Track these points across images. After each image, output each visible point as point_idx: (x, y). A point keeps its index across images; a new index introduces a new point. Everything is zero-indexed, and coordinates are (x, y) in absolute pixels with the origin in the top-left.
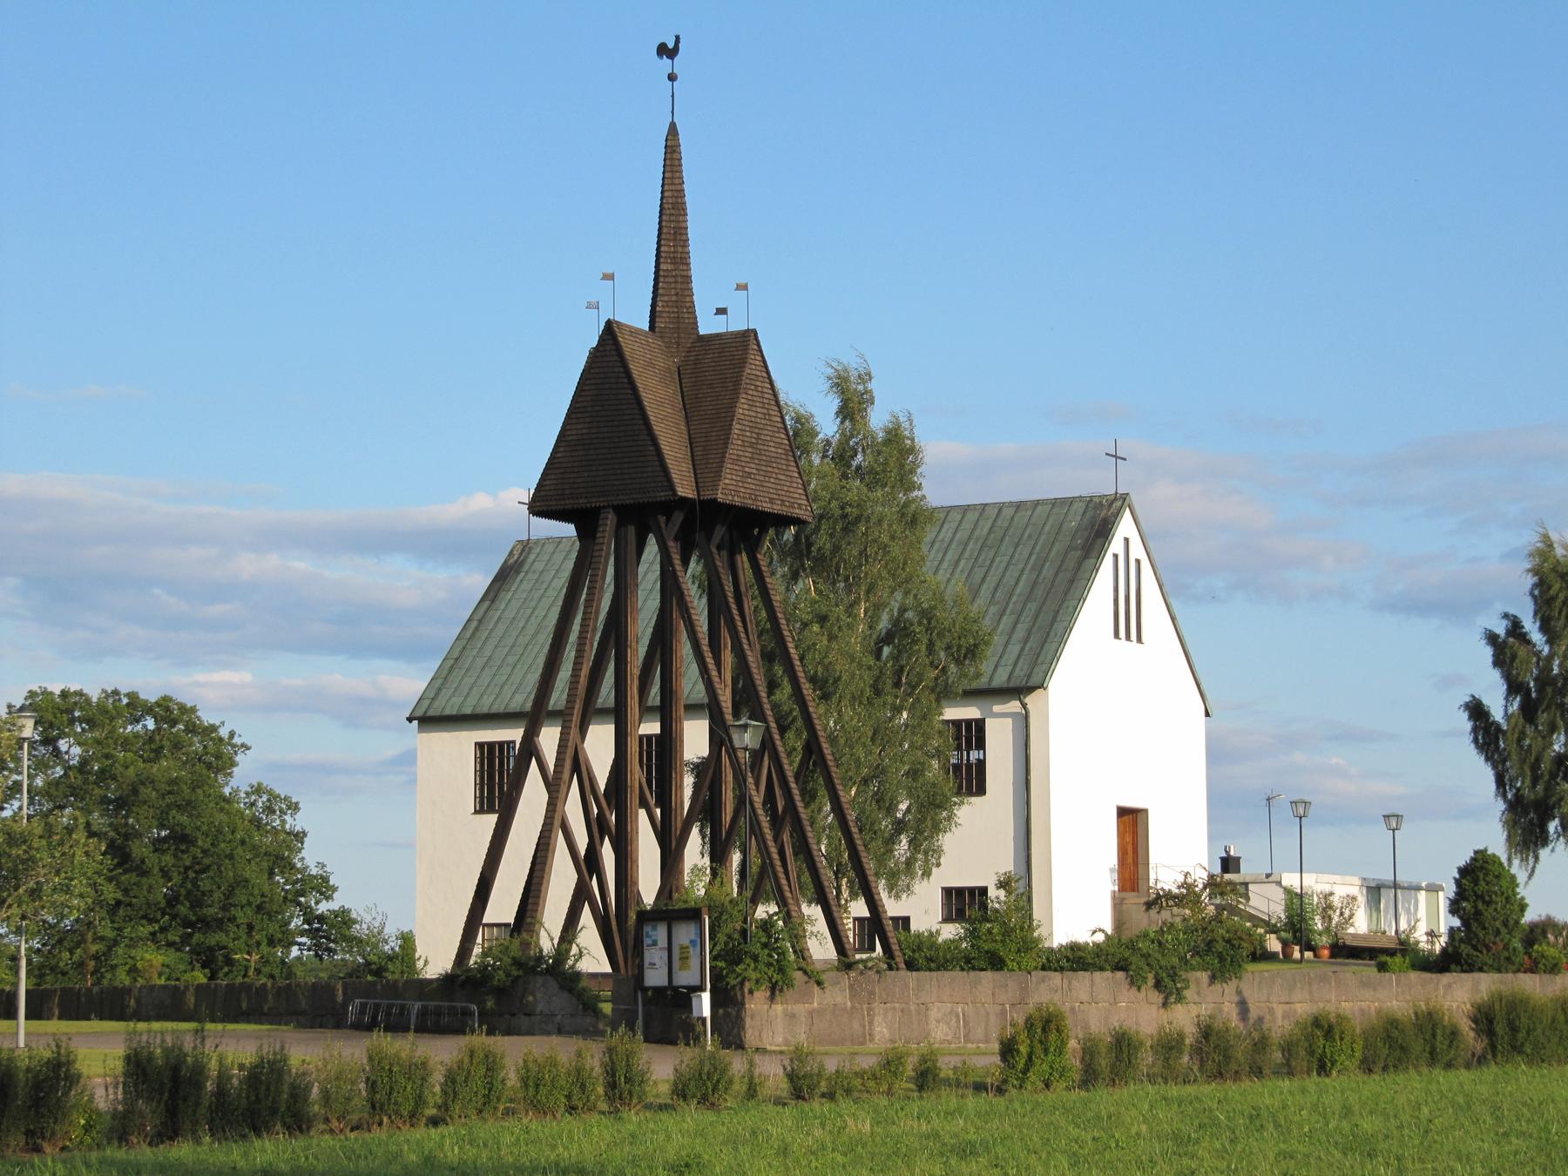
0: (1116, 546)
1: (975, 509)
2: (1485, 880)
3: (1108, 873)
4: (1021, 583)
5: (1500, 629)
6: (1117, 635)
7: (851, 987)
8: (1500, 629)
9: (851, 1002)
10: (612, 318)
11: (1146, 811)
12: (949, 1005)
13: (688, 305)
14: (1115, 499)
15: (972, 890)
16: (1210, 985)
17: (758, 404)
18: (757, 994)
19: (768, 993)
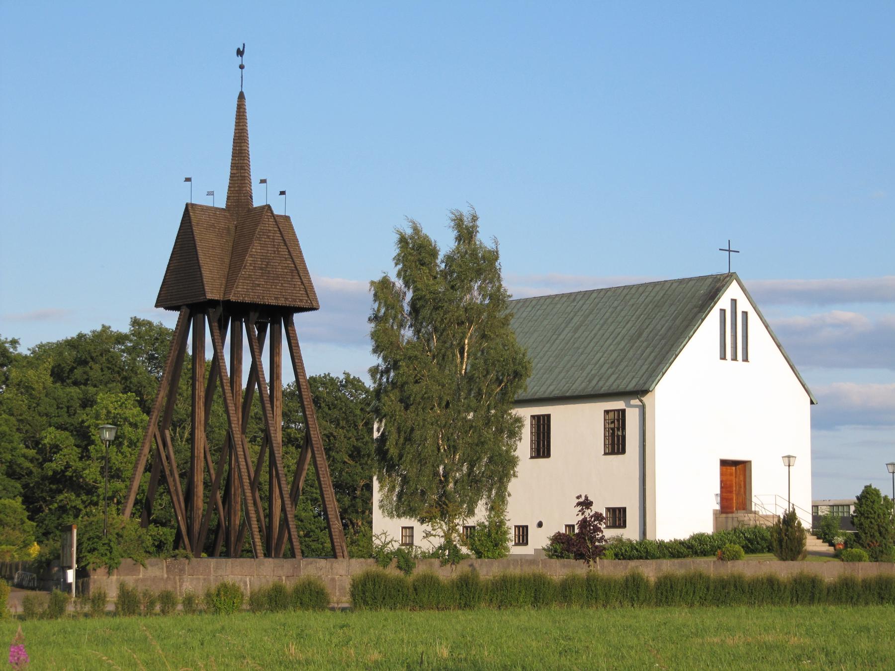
0: (724, 302)
1: (661, 284)
2: (866, 504)
3: (714, 497)
4: (663, 329)
5: (327, 374)
6: (723, 357)
7: (167, 567)
8: (327, 374)
9: (168, 575)
10: (189, 202)
11: (750, 462)
12: (239, 577)
13: (244, 192)
14: (728, 276)
15: (619, 509)
16: (441, 566)
17: (269, 246)
18: (98, 570)
19: (107, 570)
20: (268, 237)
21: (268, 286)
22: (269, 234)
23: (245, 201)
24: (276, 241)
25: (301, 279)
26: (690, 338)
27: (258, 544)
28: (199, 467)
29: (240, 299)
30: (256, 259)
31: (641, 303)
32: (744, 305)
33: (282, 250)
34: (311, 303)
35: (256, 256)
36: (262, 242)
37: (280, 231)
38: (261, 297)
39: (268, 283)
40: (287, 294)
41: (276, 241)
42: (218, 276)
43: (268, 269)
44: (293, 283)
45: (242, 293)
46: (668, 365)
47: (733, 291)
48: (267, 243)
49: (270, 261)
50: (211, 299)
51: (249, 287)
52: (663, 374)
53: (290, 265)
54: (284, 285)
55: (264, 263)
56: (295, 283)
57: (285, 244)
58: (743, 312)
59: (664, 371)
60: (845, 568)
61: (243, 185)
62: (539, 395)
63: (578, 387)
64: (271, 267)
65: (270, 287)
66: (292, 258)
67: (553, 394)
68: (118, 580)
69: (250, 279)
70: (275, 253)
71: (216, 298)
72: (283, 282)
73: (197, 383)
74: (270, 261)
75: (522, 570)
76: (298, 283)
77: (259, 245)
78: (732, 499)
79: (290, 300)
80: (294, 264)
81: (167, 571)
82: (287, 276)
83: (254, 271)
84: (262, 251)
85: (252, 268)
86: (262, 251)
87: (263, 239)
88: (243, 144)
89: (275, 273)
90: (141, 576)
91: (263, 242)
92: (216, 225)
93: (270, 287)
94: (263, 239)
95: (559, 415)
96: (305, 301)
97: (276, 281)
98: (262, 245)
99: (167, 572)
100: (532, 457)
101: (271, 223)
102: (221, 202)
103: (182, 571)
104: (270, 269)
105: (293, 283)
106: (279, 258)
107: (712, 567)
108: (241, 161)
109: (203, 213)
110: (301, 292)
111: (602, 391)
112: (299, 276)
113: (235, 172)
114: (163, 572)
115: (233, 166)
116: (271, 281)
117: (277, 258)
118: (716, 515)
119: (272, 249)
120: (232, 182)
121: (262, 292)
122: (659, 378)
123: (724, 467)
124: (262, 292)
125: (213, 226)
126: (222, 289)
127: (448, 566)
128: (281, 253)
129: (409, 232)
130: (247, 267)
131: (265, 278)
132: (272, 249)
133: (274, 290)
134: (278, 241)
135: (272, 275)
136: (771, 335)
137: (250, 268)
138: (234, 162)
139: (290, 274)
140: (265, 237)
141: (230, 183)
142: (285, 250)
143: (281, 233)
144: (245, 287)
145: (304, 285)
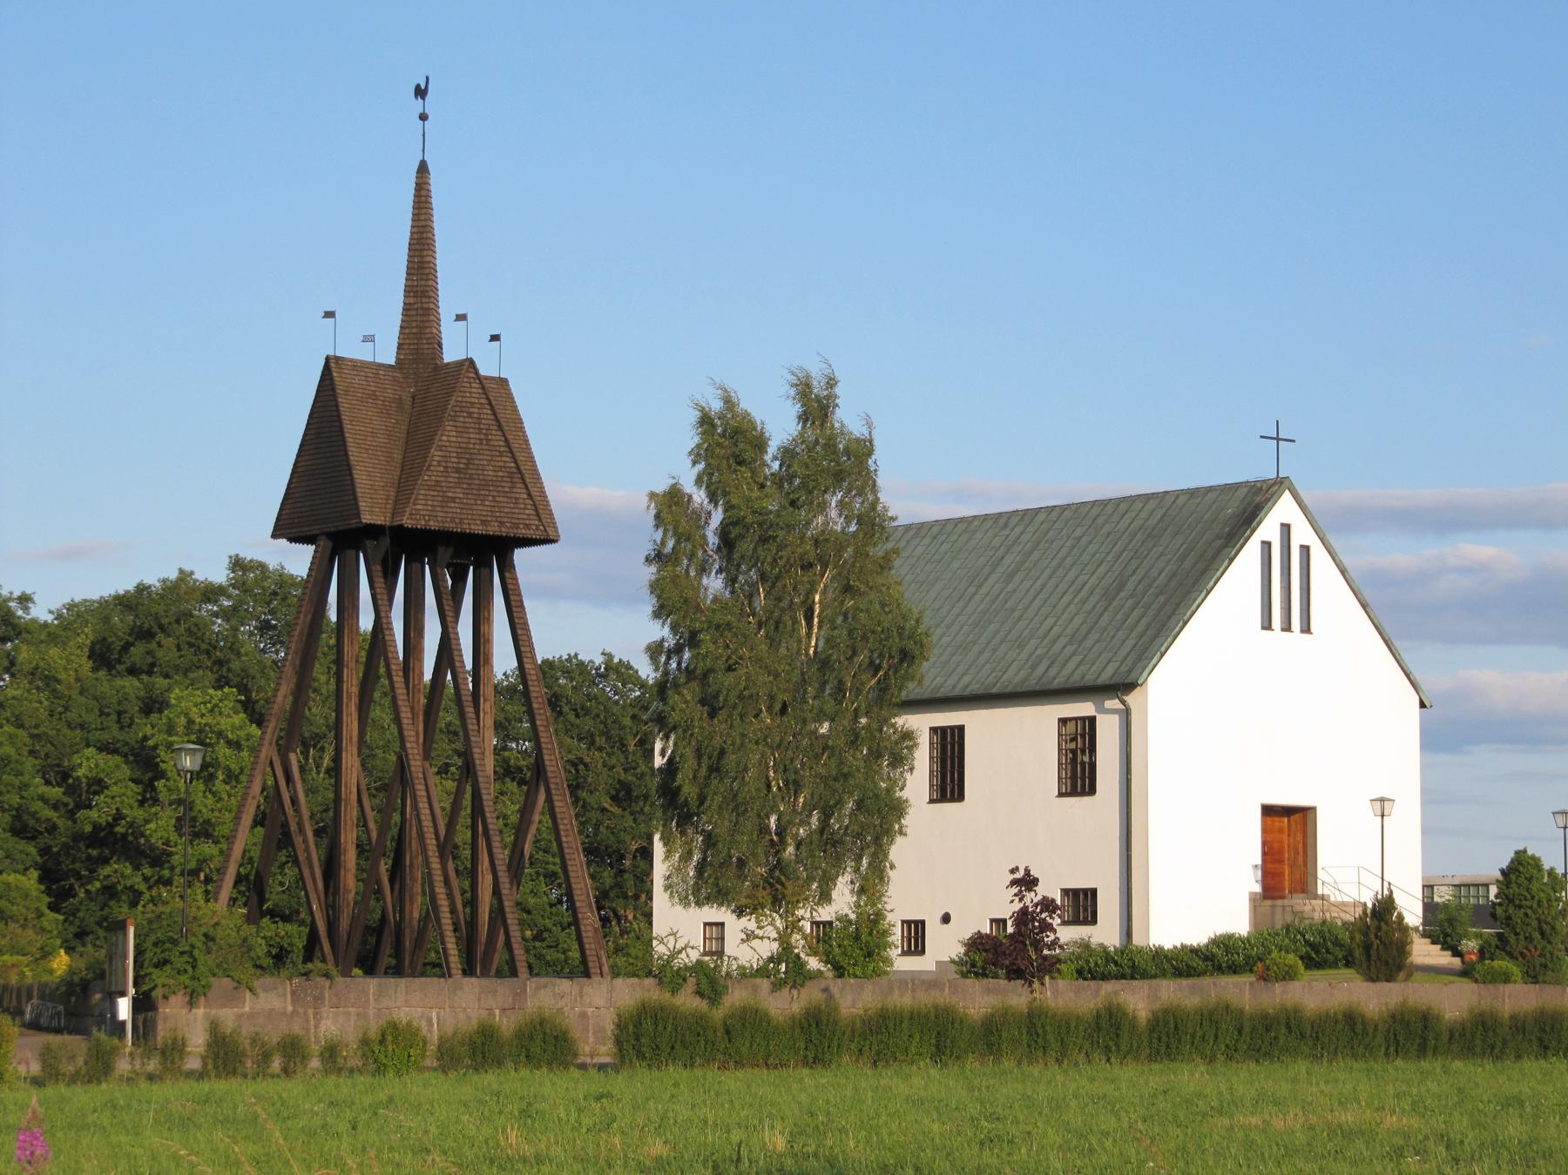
0: (1268, 529)
1: (1157, 497)
2: (1516, 883)
3: (1251, 871)
4: (1161, 577)
5: (572, 654)
6: (1267, 625)
7: (293, 993)
8: (572, 654)
9: (294, 1006)
10: (331, 353)
11: (1313, 809)
12: (420, 1010)
13: (428, 336)
14: (1275, 484)
15: (1085, 891)
16: (772, 992)
17: (471, 430)
18: (173, 999)
19: (188, 999)
20: (470, 415)
21: (470, 502)
22: (471, 410)
23: (430, 351)
24: (484, 421)
25: (527, 488)
26: (1208, 592)
27: (452, 952)
28: (348, 817)
29: (421, 524)
30: (448, 454)
31: (1122, 530)
32: (1303, 533)
33: (494, 438)
34: (545, 530)
35: (449, 449)
36: (458, 424)
37: (490, 404)
38: (457, 521)
39: (470, 496)
40: (502, 515)
41: (484, 421)
42: (381, 484)
43: (470, 471)
44: (513, 495)
45: (425, 513)
46: (1170, 639)
47: (1284, 509)
48: (467, 425)
49: (474, 457)
50: (370, 524)
51: (436, 503)
52: (1162, 655)
53: (509, 465)
54: (498, 499)
55: (462, 461)
56: (517, 495)
57: (500, 428)
58: (1302, 546)
59: (1163, 649)
60: (1480, 995)
61: (427, 324)
62: (944, 692)
63: (1012, 678)
64: (475, 467)
65: (473, 502)
66: (512, 452)
67: (969, 689)
68: (206, 1016)
69: (439, 489)
70: (481, 444)
71: (379, 523)
72: (495, 493)
73: (345, 670)
74: (474, 457)
75: (914, 998)
76: (522, 496)
77: (454, 429)
78: (1282, 874)
79: (508, 525)
80: (516, 462)
81: (293, 1001)
82: (503, 484)
83: (445, 474)
84: (459, 439)
85: (442, 469)
86: (459, 439)
87: (461, 419)
88: (425, 253)
89: (481, 477)
90: (247, 1009)
91: (462, 424)
92: (378, 394)
93: (473, 502)
94: (461, 419)
95: (980, 726)
96: (534, 527)
97: (483, 492)
98: (460, 429)
99: (293, 1001)
100: (932, 801)
101: (475, 390)
102: (387, 354)
103: (318, 999)
104: (473, 472)
105: (513, 495)
106: (488, 453)
107: (1247, 993)
108: (423, 283)
109: (355, 373)
110: (527, 512)
111: (1055, 685)
112: (525, 483)
113: (412, 300)
114: (285, 1002)
115: (409, 290)
116: (475, 492)
117: (485, 452)
118: (1255, 901)
119: (477, 436)
120: (407, 318)
121: (458, 511)
122: (1154, 661)
123: (1268, 819)
124: (458, 511)
125: (373, 395)
126: (389, 506)
127: (786, 991)
128: (492, 443)
129: (716, 405)
130: (432, 468)
131: (465, 486)
132: (477, 436)
133: (481, 508)
134: (486, 422)
135: (477, 482)
136: (1351, 587)
137: (439, 469)
138: (410, 283)
139: (509, 480)
140: (465, 414)
141: (402, 321)
142: (499, 438)
143: (492, 409)
144: (430, 503)
145: (532, 499)
